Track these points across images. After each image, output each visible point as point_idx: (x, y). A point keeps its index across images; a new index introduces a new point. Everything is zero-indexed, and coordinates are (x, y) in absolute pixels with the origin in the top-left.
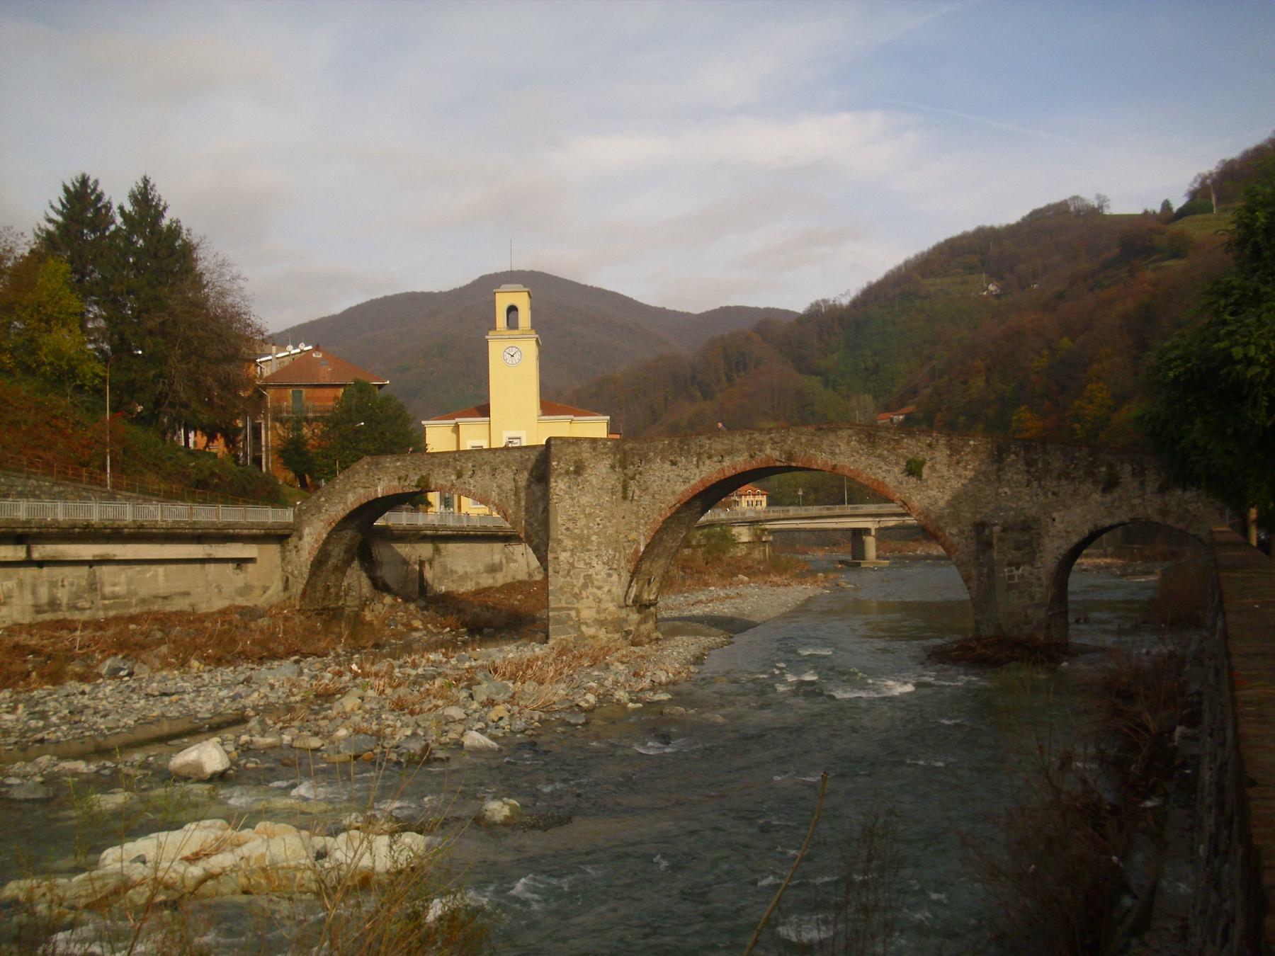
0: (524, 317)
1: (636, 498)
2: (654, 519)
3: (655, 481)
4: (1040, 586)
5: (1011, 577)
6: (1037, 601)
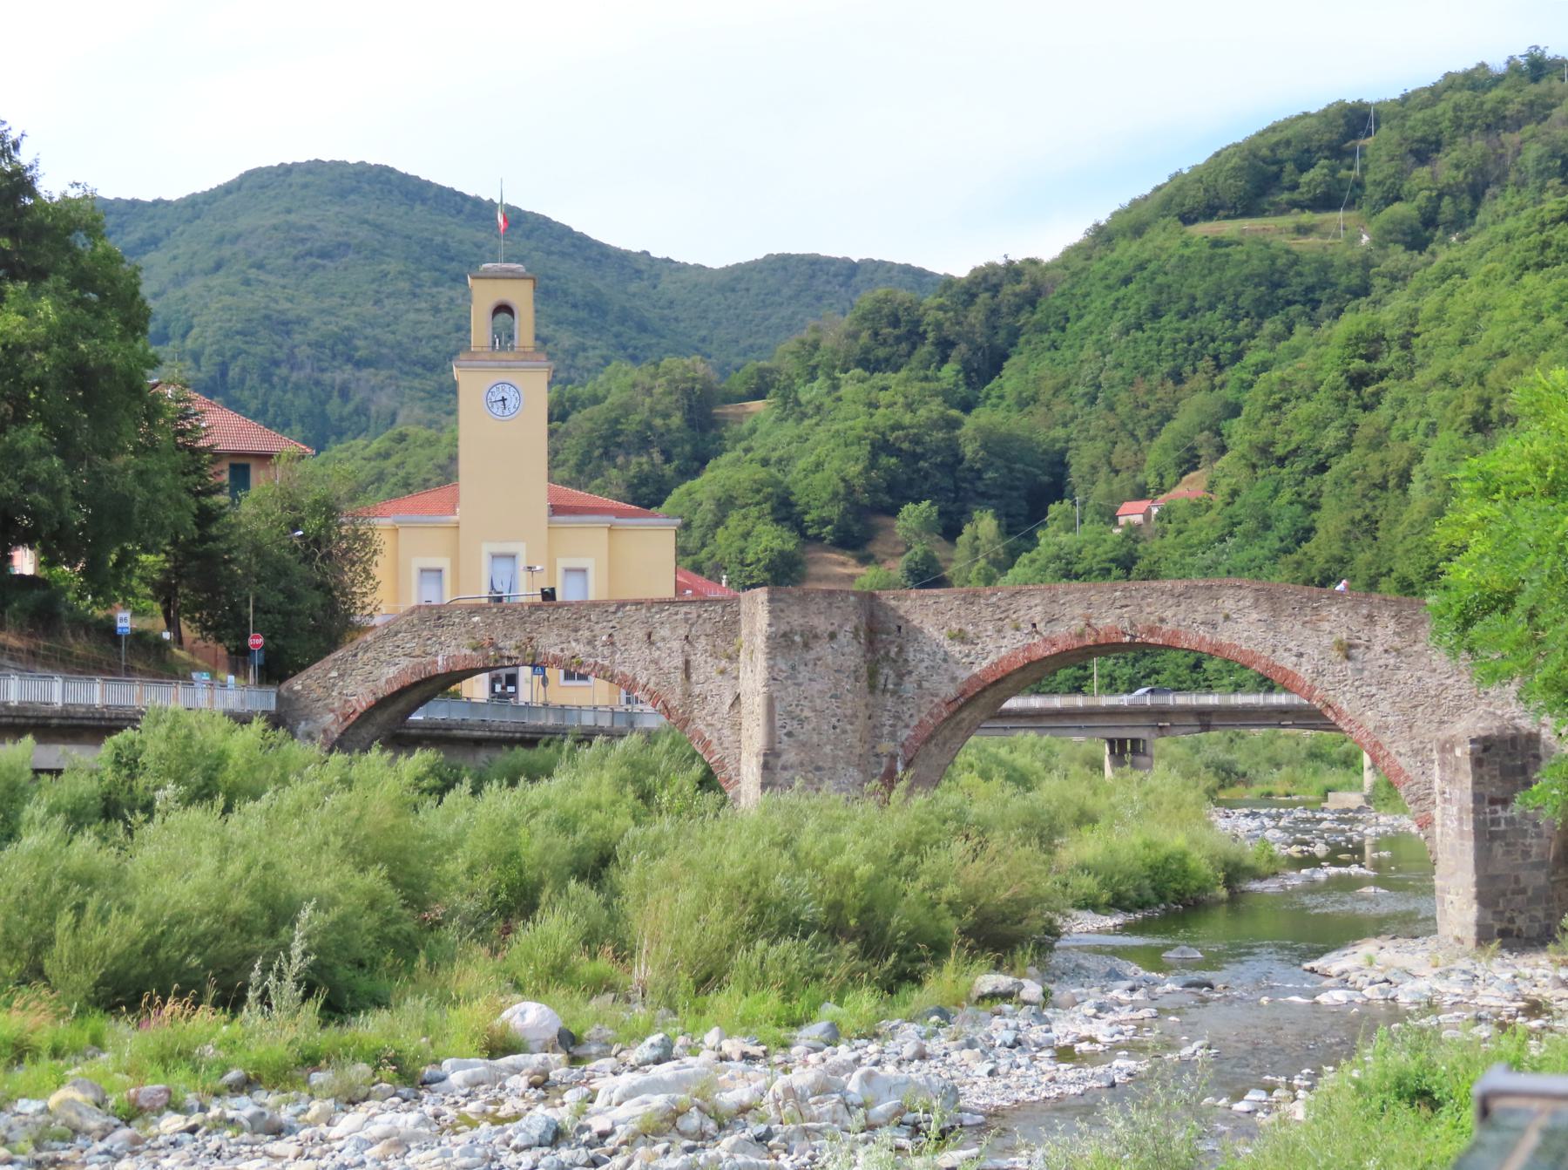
0: (524, 326)
1: (891, 687)
2: (921, 722)
3: (922, 660)
4: (1539, 835)
5: (1495, 822)
6: (1533, 859)
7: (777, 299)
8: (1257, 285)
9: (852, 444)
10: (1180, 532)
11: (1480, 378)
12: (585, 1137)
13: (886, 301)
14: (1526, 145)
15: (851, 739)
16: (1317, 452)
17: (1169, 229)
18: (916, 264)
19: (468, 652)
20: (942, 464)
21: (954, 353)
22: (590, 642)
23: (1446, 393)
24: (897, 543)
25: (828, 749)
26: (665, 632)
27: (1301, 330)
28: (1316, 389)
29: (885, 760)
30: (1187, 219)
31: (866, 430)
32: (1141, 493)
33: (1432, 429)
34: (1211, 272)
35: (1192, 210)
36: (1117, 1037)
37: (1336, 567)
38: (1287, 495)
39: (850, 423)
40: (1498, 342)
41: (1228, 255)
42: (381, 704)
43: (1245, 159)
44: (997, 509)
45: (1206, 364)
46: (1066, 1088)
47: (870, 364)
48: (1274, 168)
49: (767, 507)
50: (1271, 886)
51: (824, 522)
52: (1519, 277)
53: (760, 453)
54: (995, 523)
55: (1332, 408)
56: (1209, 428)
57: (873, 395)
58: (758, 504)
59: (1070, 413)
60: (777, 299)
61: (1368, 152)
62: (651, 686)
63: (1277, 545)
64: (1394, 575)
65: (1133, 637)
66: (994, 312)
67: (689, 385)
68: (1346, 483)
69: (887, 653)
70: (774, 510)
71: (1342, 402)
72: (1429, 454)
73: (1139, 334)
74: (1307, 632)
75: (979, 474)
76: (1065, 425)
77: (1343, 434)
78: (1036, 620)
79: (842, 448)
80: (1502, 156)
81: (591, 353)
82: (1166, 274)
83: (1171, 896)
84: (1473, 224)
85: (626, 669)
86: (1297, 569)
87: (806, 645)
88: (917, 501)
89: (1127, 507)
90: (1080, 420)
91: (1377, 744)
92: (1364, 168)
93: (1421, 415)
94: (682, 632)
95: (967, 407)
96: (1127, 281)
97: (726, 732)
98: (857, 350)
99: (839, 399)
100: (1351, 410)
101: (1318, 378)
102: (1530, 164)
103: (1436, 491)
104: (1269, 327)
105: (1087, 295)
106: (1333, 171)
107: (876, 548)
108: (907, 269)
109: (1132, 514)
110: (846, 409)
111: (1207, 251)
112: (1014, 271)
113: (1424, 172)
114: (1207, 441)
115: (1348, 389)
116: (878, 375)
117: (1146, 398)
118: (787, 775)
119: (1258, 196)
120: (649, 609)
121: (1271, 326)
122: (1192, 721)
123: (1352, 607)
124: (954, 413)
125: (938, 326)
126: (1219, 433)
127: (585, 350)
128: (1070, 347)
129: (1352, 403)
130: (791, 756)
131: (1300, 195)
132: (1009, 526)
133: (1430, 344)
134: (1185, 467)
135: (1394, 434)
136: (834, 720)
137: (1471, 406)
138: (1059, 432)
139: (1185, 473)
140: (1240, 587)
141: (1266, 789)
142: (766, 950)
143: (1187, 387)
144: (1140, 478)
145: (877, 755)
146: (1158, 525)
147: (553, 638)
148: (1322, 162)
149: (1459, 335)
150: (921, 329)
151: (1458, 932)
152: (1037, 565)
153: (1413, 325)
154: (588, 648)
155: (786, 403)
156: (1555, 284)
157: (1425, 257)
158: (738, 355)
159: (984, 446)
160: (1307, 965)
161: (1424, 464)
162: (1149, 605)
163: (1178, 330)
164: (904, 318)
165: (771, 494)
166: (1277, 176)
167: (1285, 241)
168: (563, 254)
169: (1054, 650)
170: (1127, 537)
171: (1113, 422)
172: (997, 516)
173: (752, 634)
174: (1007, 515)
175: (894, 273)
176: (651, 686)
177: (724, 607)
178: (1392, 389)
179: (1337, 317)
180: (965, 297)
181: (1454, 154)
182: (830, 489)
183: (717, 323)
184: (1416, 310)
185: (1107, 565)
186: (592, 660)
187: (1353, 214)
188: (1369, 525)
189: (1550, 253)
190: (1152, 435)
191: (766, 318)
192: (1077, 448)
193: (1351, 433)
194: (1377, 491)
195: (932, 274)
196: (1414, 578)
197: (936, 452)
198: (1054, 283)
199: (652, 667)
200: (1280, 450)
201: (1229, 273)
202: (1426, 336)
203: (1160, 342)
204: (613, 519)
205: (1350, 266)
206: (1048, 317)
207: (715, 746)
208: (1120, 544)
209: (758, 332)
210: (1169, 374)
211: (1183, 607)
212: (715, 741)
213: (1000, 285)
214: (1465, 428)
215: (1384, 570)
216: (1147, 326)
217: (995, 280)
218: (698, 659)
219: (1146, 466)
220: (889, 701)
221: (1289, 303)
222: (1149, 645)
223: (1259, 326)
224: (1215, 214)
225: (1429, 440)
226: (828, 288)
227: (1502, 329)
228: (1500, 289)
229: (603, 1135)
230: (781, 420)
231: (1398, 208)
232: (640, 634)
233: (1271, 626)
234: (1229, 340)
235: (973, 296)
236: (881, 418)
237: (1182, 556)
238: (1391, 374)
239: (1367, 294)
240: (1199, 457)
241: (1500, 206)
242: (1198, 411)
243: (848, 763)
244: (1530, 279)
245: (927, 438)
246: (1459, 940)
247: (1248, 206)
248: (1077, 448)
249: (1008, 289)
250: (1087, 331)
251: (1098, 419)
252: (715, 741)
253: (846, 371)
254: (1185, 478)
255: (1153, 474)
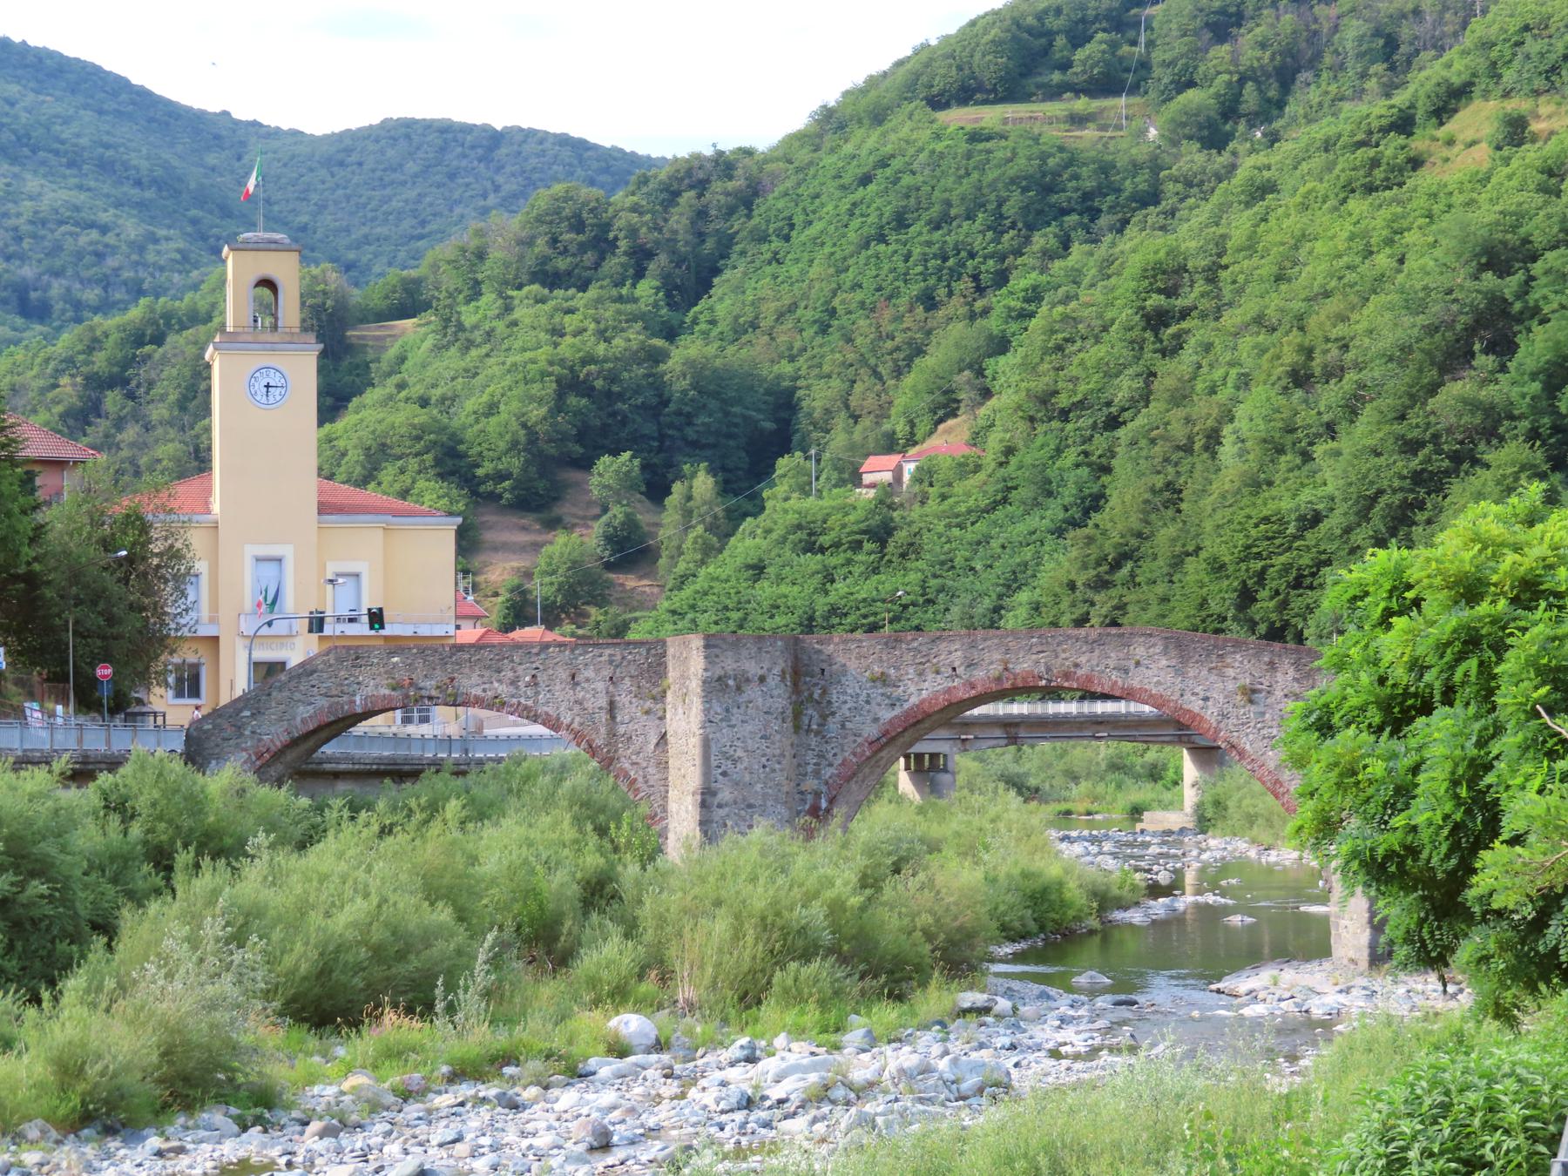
2: (845, 760)
7: (397, 176)
8: (1025, 190)
9: (533, 381)
10: (944, 497)
11: (1300, 323)
12: (768, 1103)
13: (566, 199)
14: (1345, 20)
15: (780, 777)
16: (1109, 404)
17: (916, 117)
18: (576, 133)
19: (387, 692)
20: (644, 406)
21: (652, 266)
22: (514, 683)
23: (1261, 338)
24: (590, 503)
25: (758, 787)
26: (590, 673)
27: (1077, 250)
28: (1105, 329)
29: (810, 798)
30: (938, 102)
31: (551, 363)
32: (890, 445)
33: (1245, 382)
34: (968, 174)
35: (941, 94)
36: (1090, 1042)
37: (1134, 542)
38: (1071, 456)
39: (529, 355)
40: (1320, 279)
41: (989, 152)
42: (294, 743)
43: (1008, 31)
44: (711, 462)
45: (965, 285)
46: (1082, 1075)
47: (551, 279)
48: (1043, 41)
49: (429, 458)
50: (1136, 917)
51: (501, 477)
52: (1344, 201)
53: (417, 390)
54: (710, 481)
55: (1125, 352)
56: (970, 366)
57: (557, 319)
58: (416, 455)
59: (798, 345)
60: (397, 176)
61: (1155, 24)
62: (575, 726)
63: (1061, 515)
64: (1203, 555)
65: (1049, 681)
66: (702, 214)
67: (318, 300)
68: (1143, 443)
69: (811, 695)
70: (438, 462)
71: (1138, 346)
72: (1241, 412)
73: (882, 247)
74: (1213, 678)
75: (689, 419)
76: (792, 359)
77: (1139, 384)
78: (956, 664)
79: (522, 386)
80: (1315, 33)
81: (163, 246)
82: (914, 173)
83: (1050, 926)
84: (1281, 116)
85: (550, 710)
86: (1088, 545)
87: (739, 688)
88: (615, 453)
89: (871, 462)
90: (809, 353)
91: (1277, 782)
92: (1151, 44)
93: (1231, 364)
94: (607, 673)
95: (671, 334)
96: (866, 180)
97: (651, 770)
98: (530, 261)
99: (515, 323)
100: (1148, 355)
101: (1109, 315)
102: (1349, 45)
103: (1251, 457)
104: (1039, 241)
105: (817, 196)
106: (1114, 46)
107: (564, 509)
108: (564, 141)
109: (878, 470)
110: (523, 337)
111: (964, 147)
112: (724, 164)
113: (1223, 50)
114: (969, 382)
115: (1144, 329)
116: (559, 293)
117: (891, 328)
118: (722, 812)
119: (1022, 75)
120: (572, 651)
121: (1042, 241)
122: (998, 733)
123: (1254, 655)
124: (658, 342)
125: (633, 232)
126: (980, 373)
127: (156, 241)
128: (797, 260)
129: (1149, 347)
130: (725, 795)
131: (1076, 73)
132: (726, 482)
133: (1241, 278)
134: (941, 413)
135: (1200, 386)
136: (764, 760)
137: (1290, 357)
138: (786, 368)
139: (941, 421)
140: (1151, 635)
141: (1064, 806)
142: (798, 971)
143: (941, 313)
144: (887, 427)
145: (802, 793)
146: (917, 488)
147: (475, 679)
148: (1100, 36)
149: (1275, 269)
150: (611, 235)
151: (1351, 954)
152: (774, 536)
153: (1220, 255)
154: (512, 689)
155: (445, 327)
156: (1385, 213)
157: (1223, 159)
158: (349, 248)
159: (695, 386)
160: (1214, 987)
161: (1236, 424)
162: (1064, 651)
163: (929, 244)
164: (590, 220)
165: (435, 443)
166: (1046, 51)
167: (1055, 134)
168: (119, 114)
169: (973, 693)
170: (881, 502)
171: (851, 357)
172: (712, 471)
173: (684, 677)
174: (724, 469)
175: (547, 145)
176: (575, 726)
177: (648, 651)
178: (1198, 332)
179: (1120, 231)
180: (665, 195)
181: (1258, 30)
182: (508, 437)
183: (322, 207)
184: (1224, 237)
185: (858, 537)
186: (514, 701)
187: (1136, 100)
188: (1171, 495)
189: (1379, 174)
190: (898, 373)
191: (386, 200)
192: (808, 387)
193: (1148, 384)
194: (1181, 454)
195: (595, 147)
196: (1227, 559)
197: (637, 391)
198: (774, 176)
199: (577, 708)
200: (1063, 401)
201: (991, 175)
202: (1236, 268)
203: (907, 258)
204: (390, 518)
205: (1136, 167)
206: (768, 222)
207: (640, 783)
208: (873, 512)
209: (373, 219)
210: (918, 298)
211: (1097, 653)
212: (640, 779)
213: (708, 181)
214: (1284, 382)
215: (1191, 548)
216: (892, 238)
217: (701, 175)
218: (623, 699)
219: (893, 411)
220: (813, 741)
221: (1065, 212)
222: (1063, 688)
223: (1027, 240)
224: (971, 98)
225: (1241, 394)
226: (464, 163)
227: (1323, 266)
228: (1322, 218)
229: (781, 1102)
230: (439, 348)
231: (1192, 96)
232: (563, 674)
233: (1180, 672)
234: (991, 256)
235: (677, 194)
236: (568, 348)
237: (949, 526)
238: (1194, 313)
239: (1157, 203)
240: (959, 401)
241: (1314, 95)
242: (957, 345)
243: (776, 800)
244: (1357, 205)
245: (626, 375)
246: (1352, 961)
247: (1009, 90)
248: (808, 387)
249: (717, 186)
250: (817, 242)
251: (833, 354)
252: (640, 779)
253: (520, 287)
254: (941, 427)
255: (902, 421)
